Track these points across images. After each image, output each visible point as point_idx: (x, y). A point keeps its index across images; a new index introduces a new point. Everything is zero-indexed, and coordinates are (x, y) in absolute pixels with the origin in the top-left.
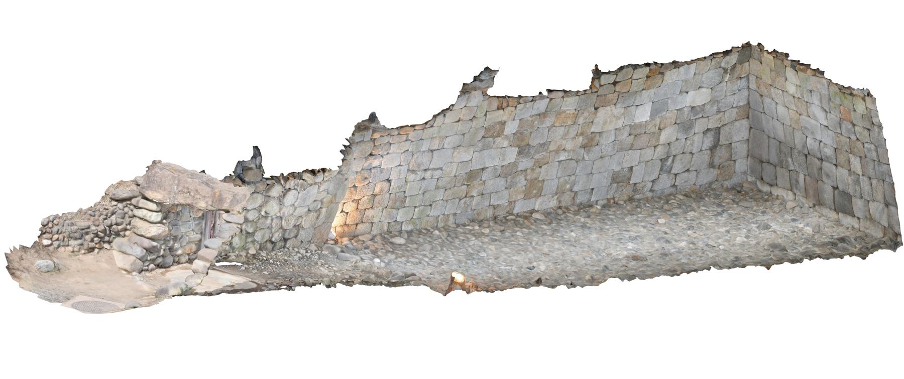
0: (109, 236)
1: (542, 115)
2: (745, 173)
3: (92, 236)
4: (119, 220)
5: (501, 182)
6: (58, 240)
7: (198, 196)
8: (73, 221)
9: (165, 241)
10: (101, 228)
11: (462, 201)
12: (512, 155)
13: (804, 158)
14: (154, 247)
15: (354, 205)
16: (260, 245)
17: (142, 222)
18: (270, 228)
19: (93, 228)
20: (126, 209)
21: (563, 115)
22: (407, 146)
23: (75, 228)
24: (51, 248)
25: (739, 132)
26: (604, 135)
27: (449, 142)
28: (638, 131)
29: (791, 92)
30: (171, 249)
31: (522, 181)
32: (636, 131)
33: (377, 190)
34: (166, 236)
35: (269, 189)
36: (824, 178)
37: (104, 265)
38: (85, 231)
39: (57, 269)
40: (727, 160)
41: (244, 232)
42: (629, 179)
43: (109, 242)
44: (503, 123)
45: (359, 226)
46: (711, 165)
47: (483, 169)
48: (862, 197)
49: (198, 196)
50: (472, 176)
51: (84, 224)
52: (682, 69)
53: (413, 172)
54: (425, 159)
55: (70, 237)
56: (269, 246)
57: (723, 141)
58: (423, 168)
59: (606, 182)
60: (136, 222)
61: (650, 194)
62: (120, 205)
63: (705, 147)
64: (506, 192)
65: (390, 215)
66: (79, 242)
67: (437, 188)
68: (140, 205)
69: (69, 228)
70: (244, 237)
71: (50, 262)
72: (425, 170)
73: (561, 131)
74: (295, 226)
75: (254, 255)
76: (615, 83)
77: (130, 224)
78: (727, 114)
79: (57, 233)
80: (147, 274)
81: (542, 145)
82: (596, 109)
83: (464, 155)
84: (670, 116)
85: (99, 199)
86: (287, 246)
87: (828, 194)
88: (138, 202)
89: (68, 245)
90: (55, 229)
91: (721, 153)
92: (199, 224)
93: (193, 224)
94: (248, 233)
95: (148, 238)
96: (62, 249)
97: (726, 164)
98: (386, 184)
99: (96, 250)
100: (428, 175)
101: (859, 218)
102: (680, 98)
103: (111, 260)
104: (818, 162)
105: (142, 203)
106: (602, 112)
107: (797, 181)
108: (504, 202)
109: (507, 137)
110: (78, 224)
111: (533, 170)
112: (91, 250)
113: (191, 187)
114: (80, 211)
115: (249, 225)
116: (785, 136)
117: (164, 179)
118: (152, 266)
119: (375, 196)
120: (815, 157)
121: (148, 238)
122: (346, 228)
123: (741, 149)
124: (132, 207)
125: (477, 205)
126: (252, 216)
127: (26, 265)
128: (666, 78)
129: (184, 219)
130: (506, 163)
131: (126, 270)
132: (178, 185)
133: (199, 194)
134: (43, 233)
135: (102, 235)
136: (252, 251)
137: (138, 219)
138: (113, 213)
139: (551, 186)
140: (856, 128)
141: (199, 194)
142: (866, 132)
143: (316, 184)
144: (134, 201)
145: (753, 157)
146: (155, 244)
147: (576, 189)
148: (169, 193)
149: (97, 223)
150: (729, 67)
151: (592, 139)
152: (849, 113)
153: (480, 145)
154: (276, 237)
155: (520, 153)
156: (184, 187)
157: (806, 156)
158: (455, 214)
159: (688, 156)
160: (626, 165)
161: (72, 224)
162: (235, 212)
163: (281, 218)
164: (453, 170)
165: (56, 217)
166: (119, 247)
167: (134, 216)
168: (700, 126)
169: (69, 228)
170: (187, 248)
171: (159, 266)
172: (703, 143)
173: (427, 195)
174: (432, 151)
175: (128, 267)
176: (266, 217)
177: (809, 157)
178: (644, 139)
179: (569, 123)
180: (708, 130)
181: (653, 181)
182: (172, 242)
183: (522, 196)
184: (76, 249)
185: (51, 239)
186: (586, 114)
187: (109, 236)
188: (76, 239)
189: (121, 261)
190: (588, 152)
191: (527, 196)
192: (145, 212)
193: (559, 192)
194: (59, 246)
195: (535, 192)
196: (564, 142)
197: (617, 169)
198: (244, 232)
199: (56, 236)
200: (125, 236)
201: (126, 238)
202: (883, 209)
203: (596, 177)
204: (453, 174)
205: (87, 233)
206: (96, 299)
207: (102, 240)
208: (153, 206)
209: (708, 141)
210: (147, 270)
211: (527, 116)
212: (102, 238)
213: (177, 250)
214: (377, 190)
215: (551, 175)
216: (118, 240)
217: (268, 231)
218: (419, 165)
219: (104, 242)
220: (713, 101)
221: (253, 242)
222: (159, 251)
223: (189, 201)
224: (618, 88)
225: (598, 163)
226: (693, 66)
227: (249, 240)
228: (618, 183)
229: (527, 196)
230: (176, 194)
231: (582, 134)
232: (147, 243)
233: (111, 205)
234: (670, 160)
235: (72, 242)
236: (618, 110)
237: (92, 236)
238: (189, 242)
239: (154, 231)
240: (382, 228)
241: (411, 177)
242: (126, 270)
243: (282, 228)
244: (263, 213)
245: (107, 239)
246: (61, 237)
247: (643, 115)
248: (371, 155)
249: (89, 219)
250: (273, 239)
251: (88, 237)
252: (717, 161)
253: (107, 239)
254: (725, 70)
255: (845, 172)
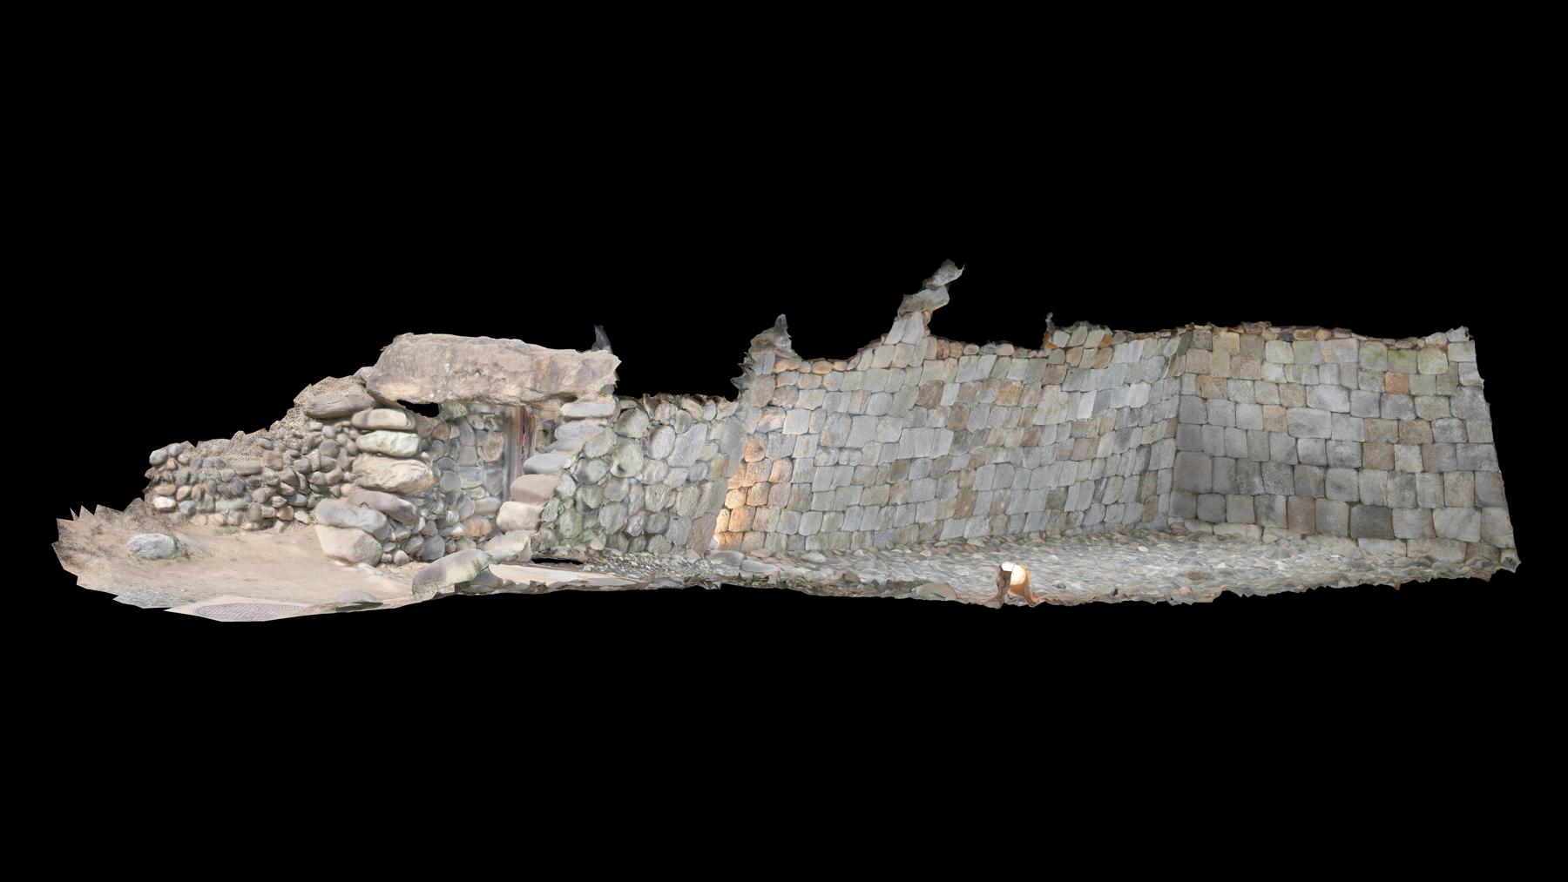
0: (307, 495)
2: (1166, 514)
3: (268, 490)
4: (327, 460)
6: (188, 497)
7: (501, 375)
8: (224, 458)
9: (429, 502)
10: (288, 473)
13: (1289, 471)
14: (404, 509)
15: (741, 496)
16: (608, 537)
17: (375, 460)
18: (625, 503)
19: (269, 473)
20: (341, 438)
21: (1008, 389)
22: (821, 399)
23: (229, 471)
24: (174, 516)
25: (1165, 456)
26: (1047, 431)
27: (876, 403)
29: (1272, 378)
30: (440, 522)
33: (774, 475)
34: (429, 490)
35: (625, 420)
36: (1330, 492)
37: (294, 550)
39: (182, 554)
41: (580, 507)
43: (308, 508)
44: (941, 385)
45: (748, 537)
47: (912, 460)
48: (1416, 506)
49: (501, 375)
50: (899, 468)
53: (825, 448)
54: (841, 427)
55: (216, 492)
56: (622, 542)
57: (1152, 467)
58: (838, 444)
59: (1041, 505)
60: (365, 463)
61: (1079, 531)
62: (328, 430)
63: (1136, 471)
64: (935, 503)
65: (790, 523)
66: (238, 502)
67: (853, 483)
68: (371, 423)
69: (214, 473)
70: (579, 516)
71: (167, 540)
72: (841, 449)
73: (1003, 413)
74: (664, 509)
75: (600, 552)
77: (350, 468)
79: (187, 482)
80: (392, 569)
81: (982, 433)
86: (650, 548)
87: (1337, 510)
88: (365, 418)
89: (213, 511)
90: (182, 473)
91: (1149, 481)
92: (495, 474)
93: (484, 475)
94: (587, 508)
95: (390, 491)
96: (200, 519)
98: (787, 464)
99: (279, 524)
101: (1405, 540)
103: (312, 541)
104: (1319, 472)
105: (377, 417)
107: (1271, 508)
108: (929, 520)
110: (235, 463)
112: (267, 523)
113: (483, 360)
115: (590, 491)
116: (1249, 448)
117: (419, 355)
118: (400, 554)
119: (770, 484)
120: (1312, 465)
121: (390, 491)
122: (728, 538)
123: (1166, 479)
124: (353, 432)
125: (901, 519)
126: (594, 471)
127: (107, 544)
128: (1116, 354)
129: (465, 459)
131: (343, 560)
132: (452, 361)
133: (501, 369)
135: (289, 489)
136: (597, 545)
137: (366, 457)
138: (313, 446)
139: (984, 502)
140: (1418, 400)
141: (501, 369)
142: (1443, 403)
143: (704, 421)
144: (357, 419)
145: (1180, 490)
146: (406, 503)
147: (1010, 511)
148: (434, 379)
149: (278, 464)
150: (1170, 356)
152: (1406, 376)
154: (634, 526)
155: (956, 441)
156: (466, 362)
157: (1293, 467)
158: (873, 532)
160: (1064, 484)
161: (222, 465)
162: (590, 396)
163: (644, 485)
164: (875, 454)
166: (329, 516)
167: (360, 451)
169: (214, 473)
170: (473, 524)
171: (415, 557)
173: (840, 494)
174: (852, 416)
175: (347, 552)
176: (620, 479)
177: (1298, 469)
181: (1085, 512)
182: (441, 505)
183: (951, 513)
184: (231, 520)
185: (174, 495)
186: (1032, 392)
187: (307, 495)
188: (231, 497)
189: (330, 541)
191: (958, 516)
192: (380, 434)
193: (992, 514)
194: (192, 513)
198: (580, 507)
199: (185, 490)
200: (340, 495)
201: (343, 500)
202: (1469, 516)
205: (256, 485)
206: (263, 601)
208: (398, 418)
210: (391, 562)
212: (289, 497)
213: (452, 526)
215: (985, 481)
216: (324, 504)
217: (622, 509)
219: (296, 508)
220: (1151, 405)
221: (597, 529)
222: (415, 521)
223: (479, 389)
224: (1069, 356)
227: (590, 524)
229: (958, 516)
230: (448, 378)
231: (1024, 425)
232: (388, 501)
235: (223, 504)
237: (268, 490)
238: (478, 514)
239: (402, 473)
240: (779, 542)
241: (823, 457)
242: (343, 560)
243: (644, 508)
244: (614, 470)
245: (300, 499)
246: (196, 490)
247: (1085, 410)
248: (770, 405)
249: (259, 455)
250: (630, 530)
251: (258, 494)
253: (300, 499)
255: (1379, 477)
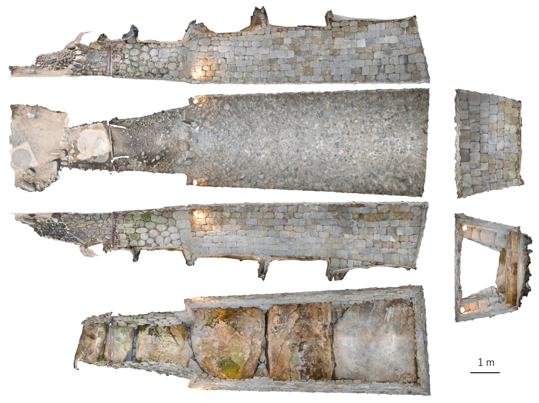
1: (304, 38)
5: (289, 66)
11: (269, 73)
12: (292, 54)
21: (315, 39)
22: (230, 43)
26: (342, 51)
28: (361, 51)
31: (301, 68)
32: (359, 51)
38: (54, 61)
40: (415, 71)
42: (361, 72)
43: (67, 66)
46: (407, 72)
51: (53, 58)
52: (377, 25)
54: (243, 50)
57: (410, 61)
64: (293, 71)
67: (253, 65)
73: (316, 46)
76: (341, 27)
78: (410, 50)
82: (334, 38)
83: (266, 51)
84: (377, 46)
85: (63, 49)
90: (41, 60)
97: (415, 72)
100: (246, 58)
102: (381, 39)
106: (337, 40)
109: (286, 45)
111: (305, 62)
112: (58, 69)
114: (54, 53)
119: (219, 65)
125: (278, 75)
129: (96, 55)
130: (289, 57)
134: (37, 62)
138: (68, 54)
147: (332, 74)
151: (335, 52)
153: (272, 47)
155: (295, 54)
159: (393, 66)
160: (358, 66)
161: (50, 58)
165: (43, 55)
168: (395, 53)
172: (399, 61)
173: (248, 68)
178: (364, 56)
179: (320, 43)
180: (401, 55)
181: (376, 76)
183: (303, 74)
190: (335, 58)
195: (309, 73)
196: (320, 51)
197: (353, 67)
203: (342, 70)
204: (260, 59)
205: (56, 62)
207: (62, 65)
209: (402, 61)
211: (295, 36)
214: (219, 62)
218: (240, 53)
220: (400, 42)
225: (341, 64)
226: (383, 24)
228: (356, 74)
233: (67, 51)
234: (383, 67)
235: (49, 65)
236: (346, 40)
241: (237, 58)
245: (65, 64)
252: (409, 70)
253: (65, 64)
254: (403, 29)
